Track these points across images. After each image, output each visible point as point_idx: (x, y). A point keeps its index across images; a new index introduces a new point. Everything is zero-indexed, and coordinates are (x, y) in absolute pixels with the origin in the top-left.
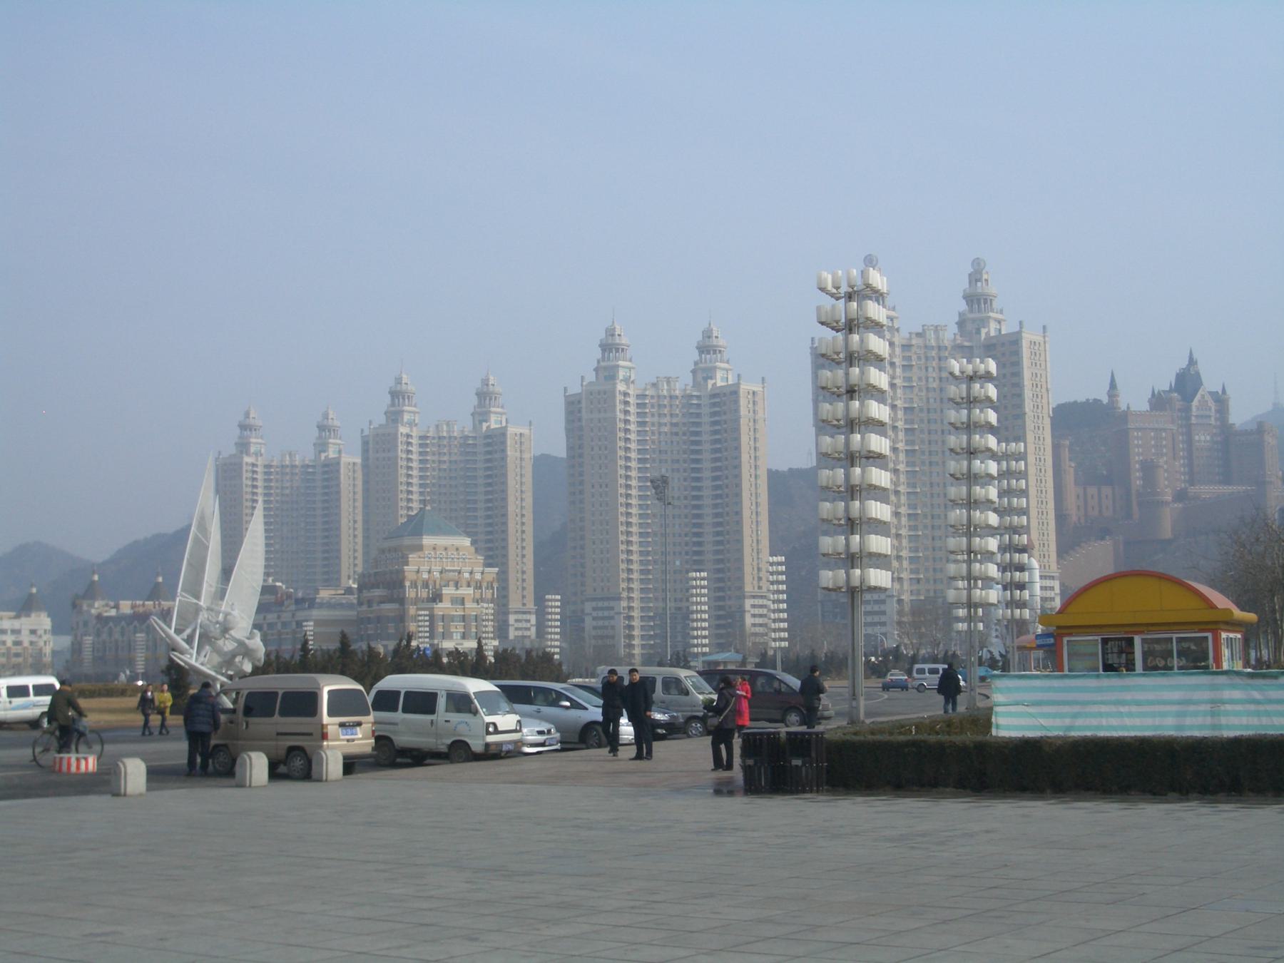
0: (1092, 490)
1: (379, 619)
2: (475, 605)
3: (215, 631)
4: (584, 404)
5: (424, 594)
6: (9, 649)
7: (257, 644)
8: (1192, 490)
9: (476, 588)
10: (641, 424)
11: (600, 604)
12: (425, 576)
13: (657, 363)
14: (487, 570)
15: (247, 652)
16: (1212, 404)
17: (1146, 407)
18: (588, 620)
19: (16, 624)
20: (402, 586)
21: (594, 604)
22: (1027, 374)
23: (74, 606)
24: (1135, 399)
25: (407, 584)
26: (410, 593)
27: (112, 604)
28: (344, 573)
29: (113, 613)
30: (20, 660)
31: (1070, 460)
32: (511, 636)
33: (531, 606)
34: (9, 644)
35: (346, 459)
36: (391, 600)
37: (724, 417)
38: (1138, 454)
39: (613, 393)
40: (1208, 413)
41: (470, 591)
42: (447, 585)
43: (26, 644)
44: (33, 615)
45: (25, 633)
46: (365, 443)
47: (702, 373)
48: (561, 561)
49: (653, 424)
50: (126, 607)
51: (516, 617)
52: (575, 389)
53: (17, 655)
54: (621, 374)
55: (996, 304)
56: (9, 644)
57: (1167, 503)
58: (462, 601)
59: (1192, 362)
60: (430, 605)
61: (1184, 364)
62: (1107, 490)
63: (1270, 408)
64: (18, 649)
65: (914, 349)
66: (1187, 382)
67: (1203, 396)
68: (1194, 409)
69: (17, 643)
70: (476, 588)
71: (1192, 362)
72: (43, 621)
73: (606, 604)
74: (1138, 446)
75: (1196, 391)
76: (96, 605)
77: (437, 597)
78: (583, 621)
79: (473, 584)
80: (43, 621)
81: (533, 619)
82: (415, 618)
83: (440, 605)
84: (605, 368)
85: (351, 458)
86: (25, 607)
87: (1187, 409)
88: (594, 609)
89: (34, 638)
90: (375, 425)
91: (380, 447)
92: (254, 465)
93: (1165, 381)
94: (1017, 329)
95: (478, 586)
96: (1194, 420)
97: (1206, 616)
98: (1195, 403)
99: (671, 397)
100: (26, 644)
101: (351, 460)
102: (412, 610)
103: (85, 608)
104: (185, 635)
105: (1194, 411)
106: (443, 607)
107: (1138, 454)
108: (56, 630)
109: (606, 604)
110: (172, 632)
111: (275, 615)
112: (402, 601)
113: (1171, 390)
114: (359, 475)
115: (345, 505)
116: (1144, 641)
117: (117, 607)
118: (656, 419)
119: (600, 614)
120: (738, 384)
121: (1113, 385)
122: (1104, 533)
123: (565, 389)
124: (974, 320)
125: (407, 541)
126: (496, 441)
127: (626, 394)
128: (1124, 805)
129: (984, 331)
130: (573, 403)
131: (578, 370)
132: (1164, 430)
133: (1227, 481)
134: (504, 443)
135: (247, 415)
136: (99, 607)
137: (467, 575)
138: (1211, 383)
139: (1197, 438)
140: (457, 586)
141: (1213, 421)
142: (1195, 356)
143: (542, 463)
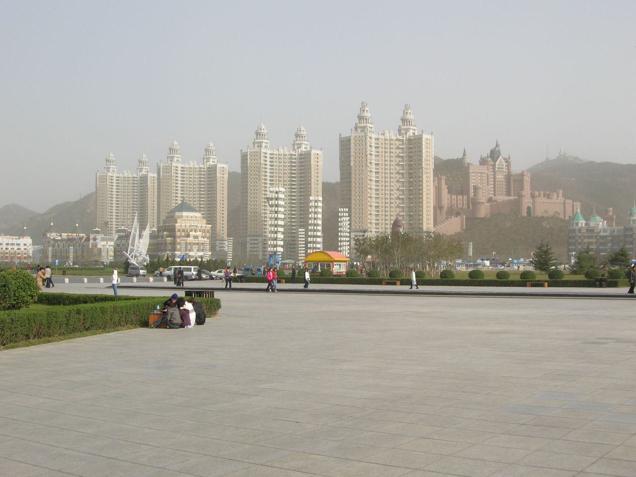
0: (454, 197)
2: (202, 239)
3: (138, 255)
5: (183, 234)
6: (15, 251)
7: (148, 258)
8: (494, 198)
9: (203, 232)
10: (271, 166)
11: (253, 238)
12: (184, 228)
14: (207, 226)
15: (144, 260)
16: (505, 164)
18: (248, 244)
19: (18, 241)
20: (175, 231)
21: (251, 238)
22: (424, 151)
23: (44, 235)
25: (177, 230)
26: (178, 234)
27: (59, 234)
29: (59, 238)
30: (26, 256)
31: (446, 184)
32: (217, 250)
34: (16, 249)
35: (150, 175)
37: (306, 164)
38: (473, 183)
40: (502, 167)
41: (201, 233)
42: (192, 231)
43: (22, 249)
44: (25, 238)
45: (22, 245)
48: (240, 217)
49: (276, 166)
50: (64, 235)
51: (219, 242)
53: (19, 254)
54: (264, 145)
56: (16, 249)
57: (483, 203)
59: (497, 145)
60: (185, 239)
63: (545, 160)
64: (18, 251)
65: (380, 140)
66: (494, 154)
67: (501, 160)
68: (497, 165)
69: (7, 249)
70: (203, 232)
71: (497, 145)
72: (28, 240)
73: (255, 238)
74: (473, 179)
76: (52, 235)
77: (188, 236)
78: (246, 244)
79: (202, 231)
80: (28, 240)
82: (180, 244)
83: (189, 239)
84: (258, 143)
86: (21, 234)
87: (494, 165)
88: (251, 240)
89: (25, 247)
92: (112, 177)
93: (486, 153)
94: (421, 133)
95: (204, 231)
96: (496, 169)
97: (331, 260)
98: (497, 163)
99: (284, 155)
100: (22, 249)
101: (152, 175)
102: (178, 240)
103: (48, 236)
104: (131, 256)
105: (497, 166)
106: (190, 240)
107: (473, 183)
108: (33, 244)
109: (255, 238)
110: (128, 255)
111: (125, 241)
114: (156, 182)
115: (150, 194)
116: (320, 264)
117: (61, 236)
118: (278, 164)
119: (253, 242)
120: (310, 151)
121: (464, 154)
122: (458, 214)
123: (241, 150)
124: (404, 129)
125: (177, 214)
127: (265, 153)
130: (343, 141)
132: (484, 173)
134: (216, 171)
136: (53, 235)
137: (200, 228)
138: (504, 153)
139: (497, 177)
141: (504, 170)
142: (499, 143)
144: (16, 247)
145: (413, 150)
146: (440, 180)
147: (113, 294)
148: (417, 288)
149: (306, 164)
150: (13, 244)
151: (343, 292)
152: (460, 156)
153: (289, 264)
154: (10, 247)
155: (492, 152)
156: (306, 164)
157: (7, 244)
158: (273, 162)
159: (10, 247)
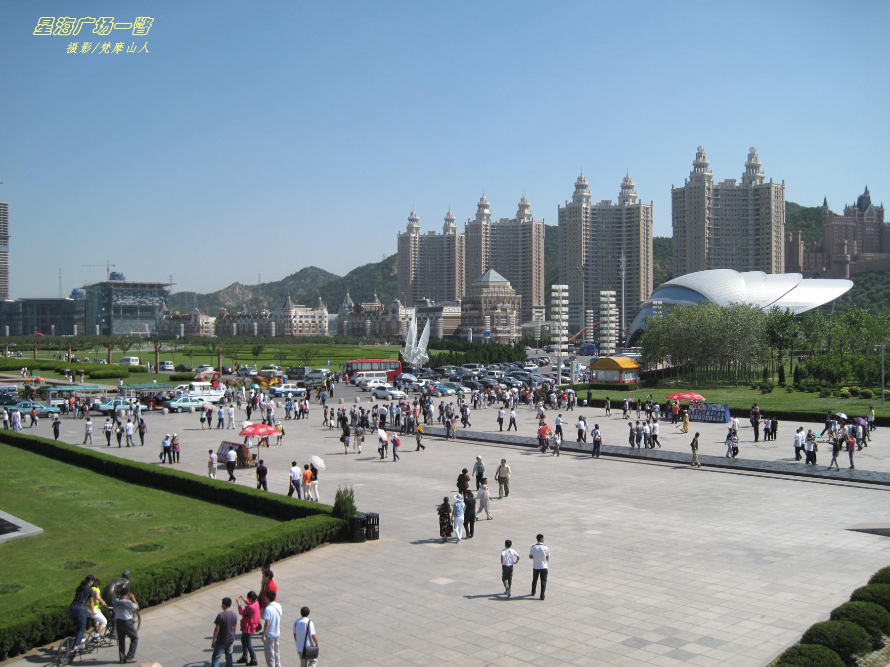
0: (812, 255)
1: (470, 317)
4: (686, 195)
13: (603, 192)
17: (841, 213)
24: (837, 208)
28: (457, 294)
33: (543, 305)
36: (476, 309)
39: (580, 208)
41: (510, 305)
46: (466, 228)
47: (623, 198)
52: (563, 206)
55: (761, 169)
58: (506, 310)
59: (867, 192)
61: (862, 192)
62: (819, 255)
66: (864, 201)
71: (867, 192)
75: (867, 206)
77: (495, 308)
81: (544, 311)
85: (460, 231)
90: (471, 220)
91: (473, 229)
93: (852, 201)
95: (513, 303)
112: (480, 310)
113: (854, 206)
121: (825, 203)
126: (527, 228)
128: (127, 460)
129: (754, 183)
131: (566, 197)
133: (880, 250)
134: (531, 229)
135: (412, 214)
138: (875, 202)
140: (503, 303)
142: (868, 189)
143: (549, 230)
144: (310, 320)
145: (759, 202)
146: (795, 235)
147: (616, 379)
148: (232, 478)
149: (634, 219)
150: (307, 317)
151: (814, 414)
152: (821, 204)
153: (75, 418)
154: (304, 320)
155: (861, 199)
156: (634, 219)
157: (301, 317)
158: (758, 199)
159: (304, 320)
